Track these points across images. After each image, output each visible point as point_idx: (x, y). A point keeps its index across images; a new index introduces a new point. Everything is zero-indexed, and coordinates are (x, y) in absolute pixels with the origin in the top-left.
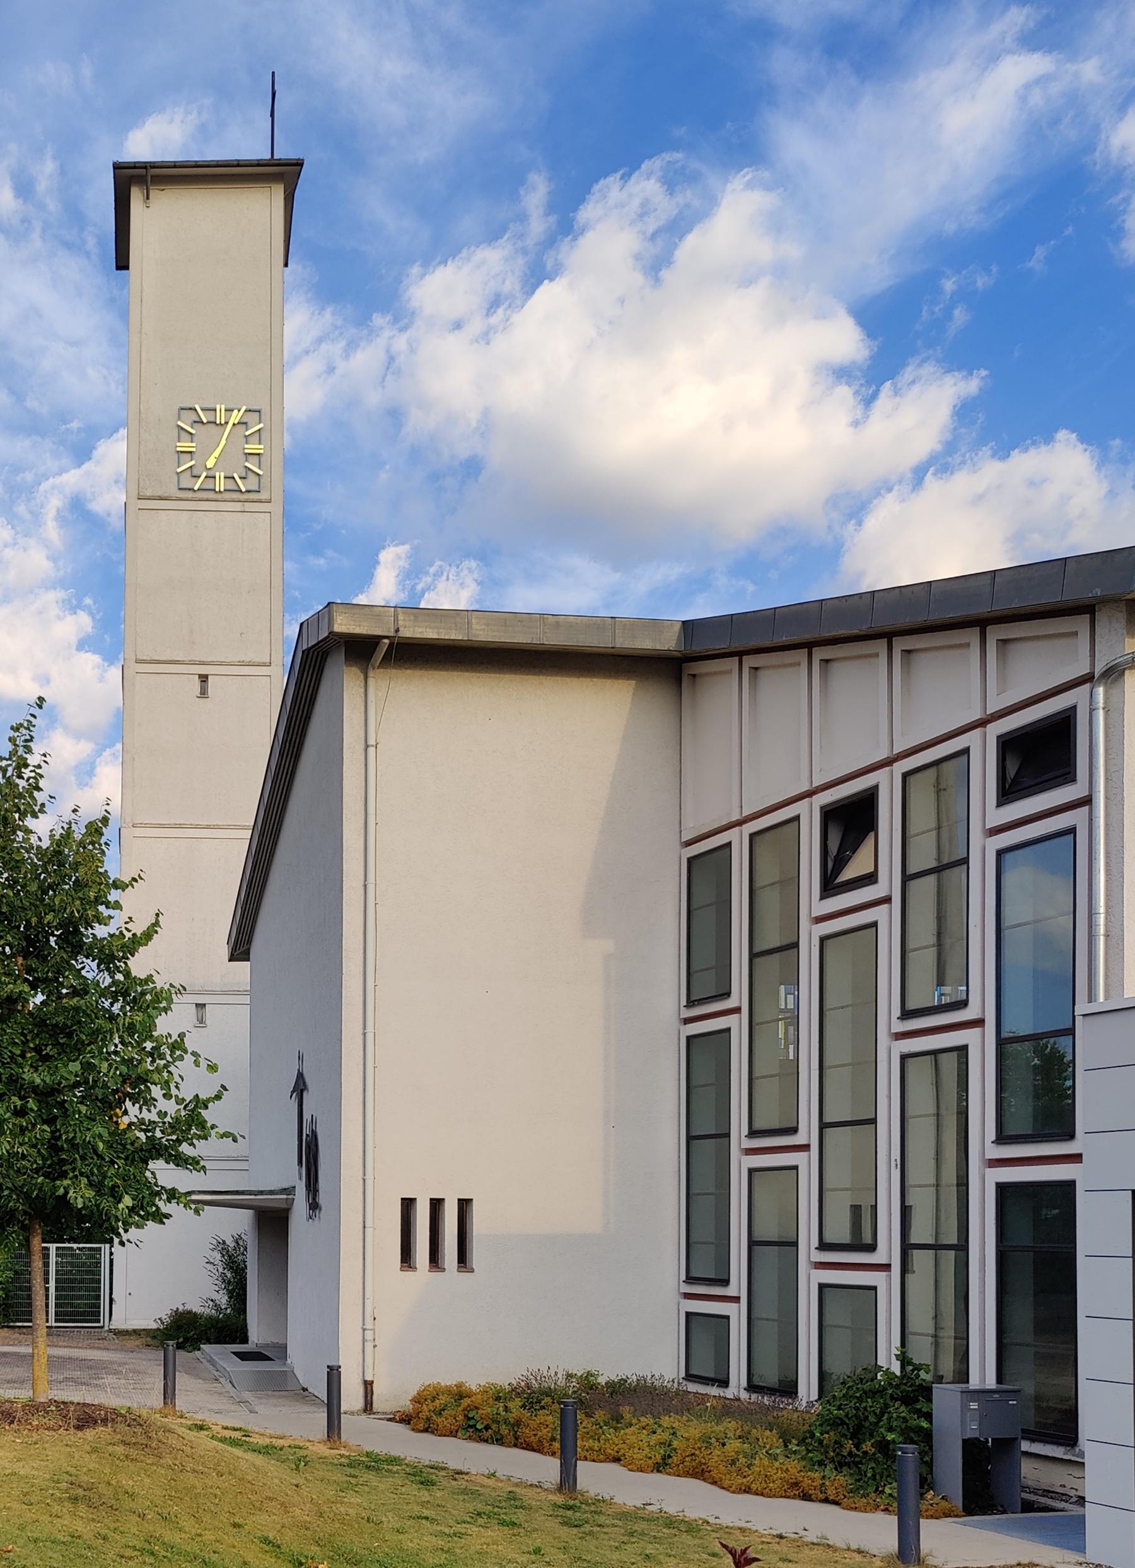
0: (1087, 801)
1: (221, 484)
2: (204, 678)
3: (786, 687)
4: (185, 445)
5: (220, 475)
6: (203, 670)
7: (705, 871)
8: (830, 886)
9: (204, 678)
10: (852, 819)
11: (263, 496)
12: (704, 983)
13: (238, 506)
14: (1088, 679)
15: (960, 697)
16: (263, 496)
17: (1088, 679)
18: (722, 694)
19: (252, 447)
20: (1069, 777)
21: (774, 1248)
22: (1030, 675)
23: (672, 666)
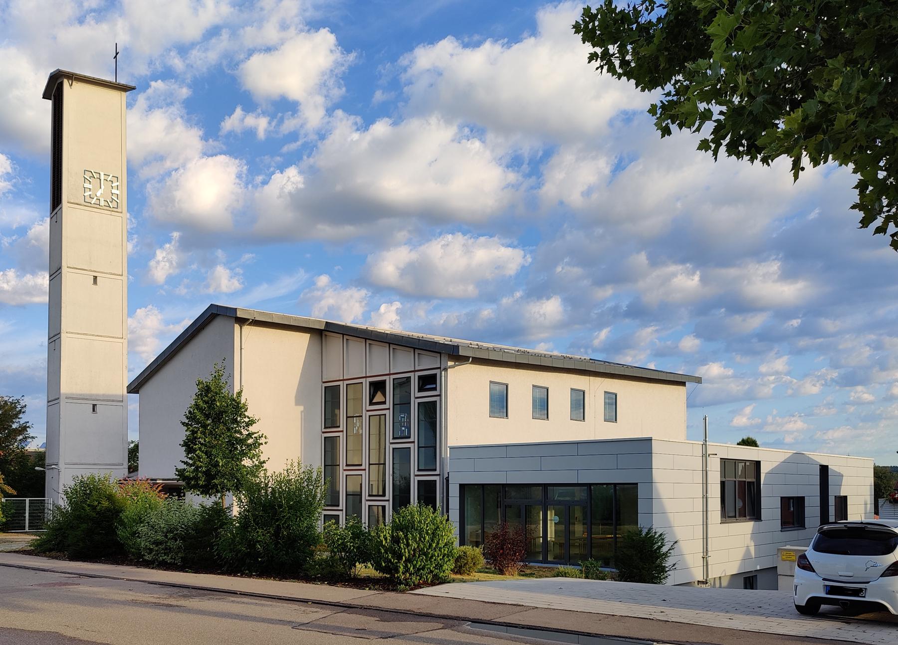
0: (440, 395)
1: (102, 203)
2: (95, 278)
3: (357, 348)
4: (87, 185)
5: (102, 200)
6: (95, 274)
7: (331, 395)
8: (371, 403)
9: (95, 278)
10: (378, 387)
11: (119, 210)
12: (331, 421)
13: (109, 213)
14: (440, 368)
15: (406, 364)
16: (119, 210)
17: (440, 368)
18: (335, 344)
19: (114, 191)
20: (435, 389)
21: (355, 498)
22: (427, 363)
23: (323, 333)
